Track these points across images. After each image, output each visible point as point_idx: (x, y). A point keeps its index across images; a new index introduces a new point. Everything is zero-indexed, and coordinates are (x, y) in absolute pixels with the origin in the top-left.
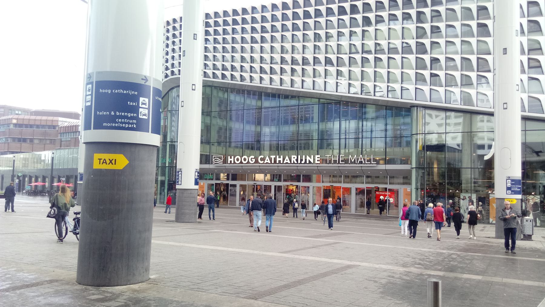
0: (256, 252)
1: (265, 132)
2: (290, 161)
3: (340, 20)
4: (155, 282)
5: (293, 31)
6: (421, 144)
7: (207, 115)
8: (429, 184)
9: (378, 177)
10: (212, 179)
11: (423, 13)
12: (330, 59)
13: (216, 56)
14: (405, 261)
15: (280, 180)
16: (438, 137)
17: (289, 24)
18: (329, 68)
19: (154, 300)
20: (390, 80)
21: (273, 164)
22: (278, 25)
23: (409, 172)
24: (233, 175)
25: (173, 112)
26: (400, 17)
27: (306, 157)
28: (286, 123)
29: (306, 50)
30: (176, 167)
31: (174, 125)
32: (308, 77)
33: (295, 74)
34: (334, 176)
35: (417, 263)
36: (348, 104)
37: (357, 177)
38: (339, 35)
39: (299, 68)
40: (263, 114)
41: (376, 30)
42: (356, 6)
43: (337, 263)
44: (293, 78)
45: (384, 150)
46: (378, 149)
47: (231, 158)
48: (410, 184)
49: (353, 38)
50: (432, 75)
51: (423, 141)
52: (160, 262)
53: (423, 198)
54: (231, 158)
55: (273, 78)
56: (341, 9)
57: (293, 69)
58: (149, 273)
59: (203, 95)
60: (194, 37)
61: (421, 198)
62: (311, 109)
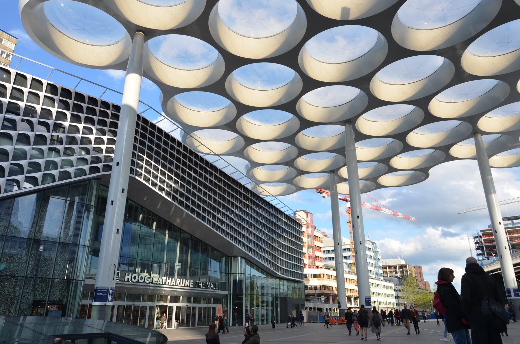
47: (129, 275)
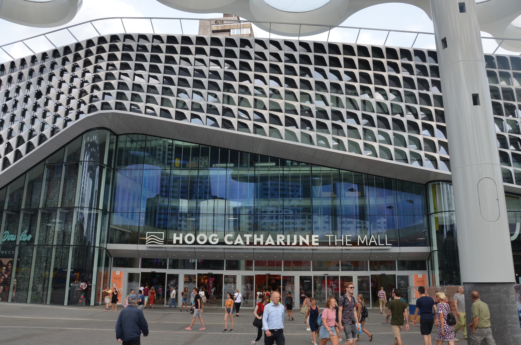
54: (260, 238)
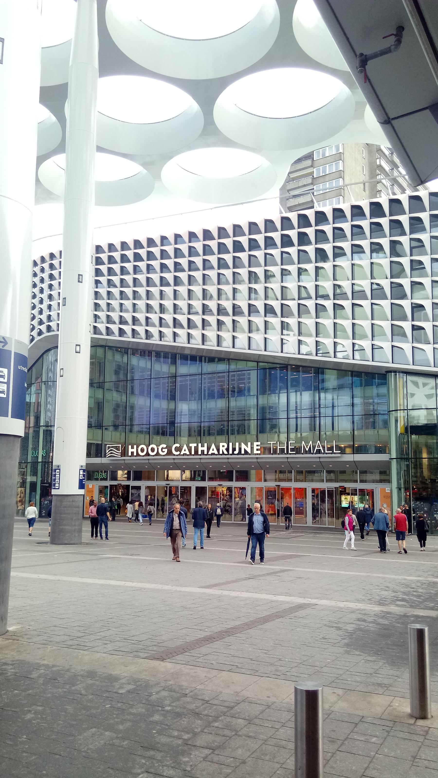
0: (166, 587)
1: (182, 409)
2: (218, 450)
3: (284, 254)
4: (15, 636)
5: (219, 268)
6: (402, 423)
7: (99, 387)
8: (416, 481)
9: (343, 472)
10: (106, 479)
11: (399, 243)
12: (271, 307)
13: (111, 304)
14: (383, 597)
15: (203, 479)
16: (428, 414)
17: (213, 259)
18: (271, 319)
19: (12, 665)
20: (356, 335)
21: (193, 455)
22: (198, 261)
23: (388, 464)
24: (135, 472)
25: (50, 383)
26: (367, 249)
27: (240, 445)
28: (211, 396)
29: (238, 295)
30: (52, 462)
31: (51, 401)
32: (241, 333)
33: (223, 327)
34: (281, 472)
35: (399, 599)
36: (299, 368)
37: (314, 472)
38: (283, 274)
39: (227, 320)
40: (178, 384)
41: (334, 266)
42: (305, 234)
43: (284, 601)
44: (220, 333)
45: (351, 433)
46: (342, 432)
47: (132, 448)
48: (389, 481)
49: (302, 277)
50: (414, 328)
51: (406, 420)
52: (25, 605)
53: (408, 502)
54: (133, 448)
55: (206, 335)
56: (285, 239)
57: (220, 321)
58: (6, 624)
59: (91, 358)
60: (79, 278)
61: (406, 501)
62: (246, 377)
